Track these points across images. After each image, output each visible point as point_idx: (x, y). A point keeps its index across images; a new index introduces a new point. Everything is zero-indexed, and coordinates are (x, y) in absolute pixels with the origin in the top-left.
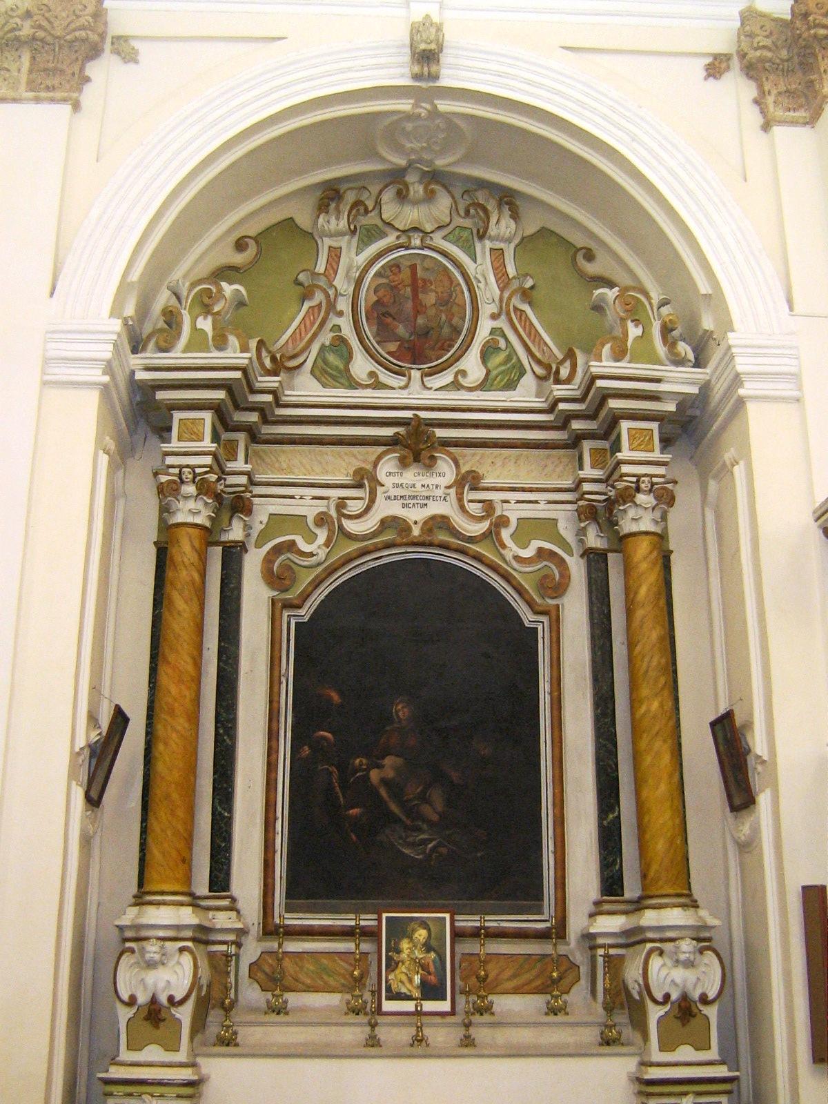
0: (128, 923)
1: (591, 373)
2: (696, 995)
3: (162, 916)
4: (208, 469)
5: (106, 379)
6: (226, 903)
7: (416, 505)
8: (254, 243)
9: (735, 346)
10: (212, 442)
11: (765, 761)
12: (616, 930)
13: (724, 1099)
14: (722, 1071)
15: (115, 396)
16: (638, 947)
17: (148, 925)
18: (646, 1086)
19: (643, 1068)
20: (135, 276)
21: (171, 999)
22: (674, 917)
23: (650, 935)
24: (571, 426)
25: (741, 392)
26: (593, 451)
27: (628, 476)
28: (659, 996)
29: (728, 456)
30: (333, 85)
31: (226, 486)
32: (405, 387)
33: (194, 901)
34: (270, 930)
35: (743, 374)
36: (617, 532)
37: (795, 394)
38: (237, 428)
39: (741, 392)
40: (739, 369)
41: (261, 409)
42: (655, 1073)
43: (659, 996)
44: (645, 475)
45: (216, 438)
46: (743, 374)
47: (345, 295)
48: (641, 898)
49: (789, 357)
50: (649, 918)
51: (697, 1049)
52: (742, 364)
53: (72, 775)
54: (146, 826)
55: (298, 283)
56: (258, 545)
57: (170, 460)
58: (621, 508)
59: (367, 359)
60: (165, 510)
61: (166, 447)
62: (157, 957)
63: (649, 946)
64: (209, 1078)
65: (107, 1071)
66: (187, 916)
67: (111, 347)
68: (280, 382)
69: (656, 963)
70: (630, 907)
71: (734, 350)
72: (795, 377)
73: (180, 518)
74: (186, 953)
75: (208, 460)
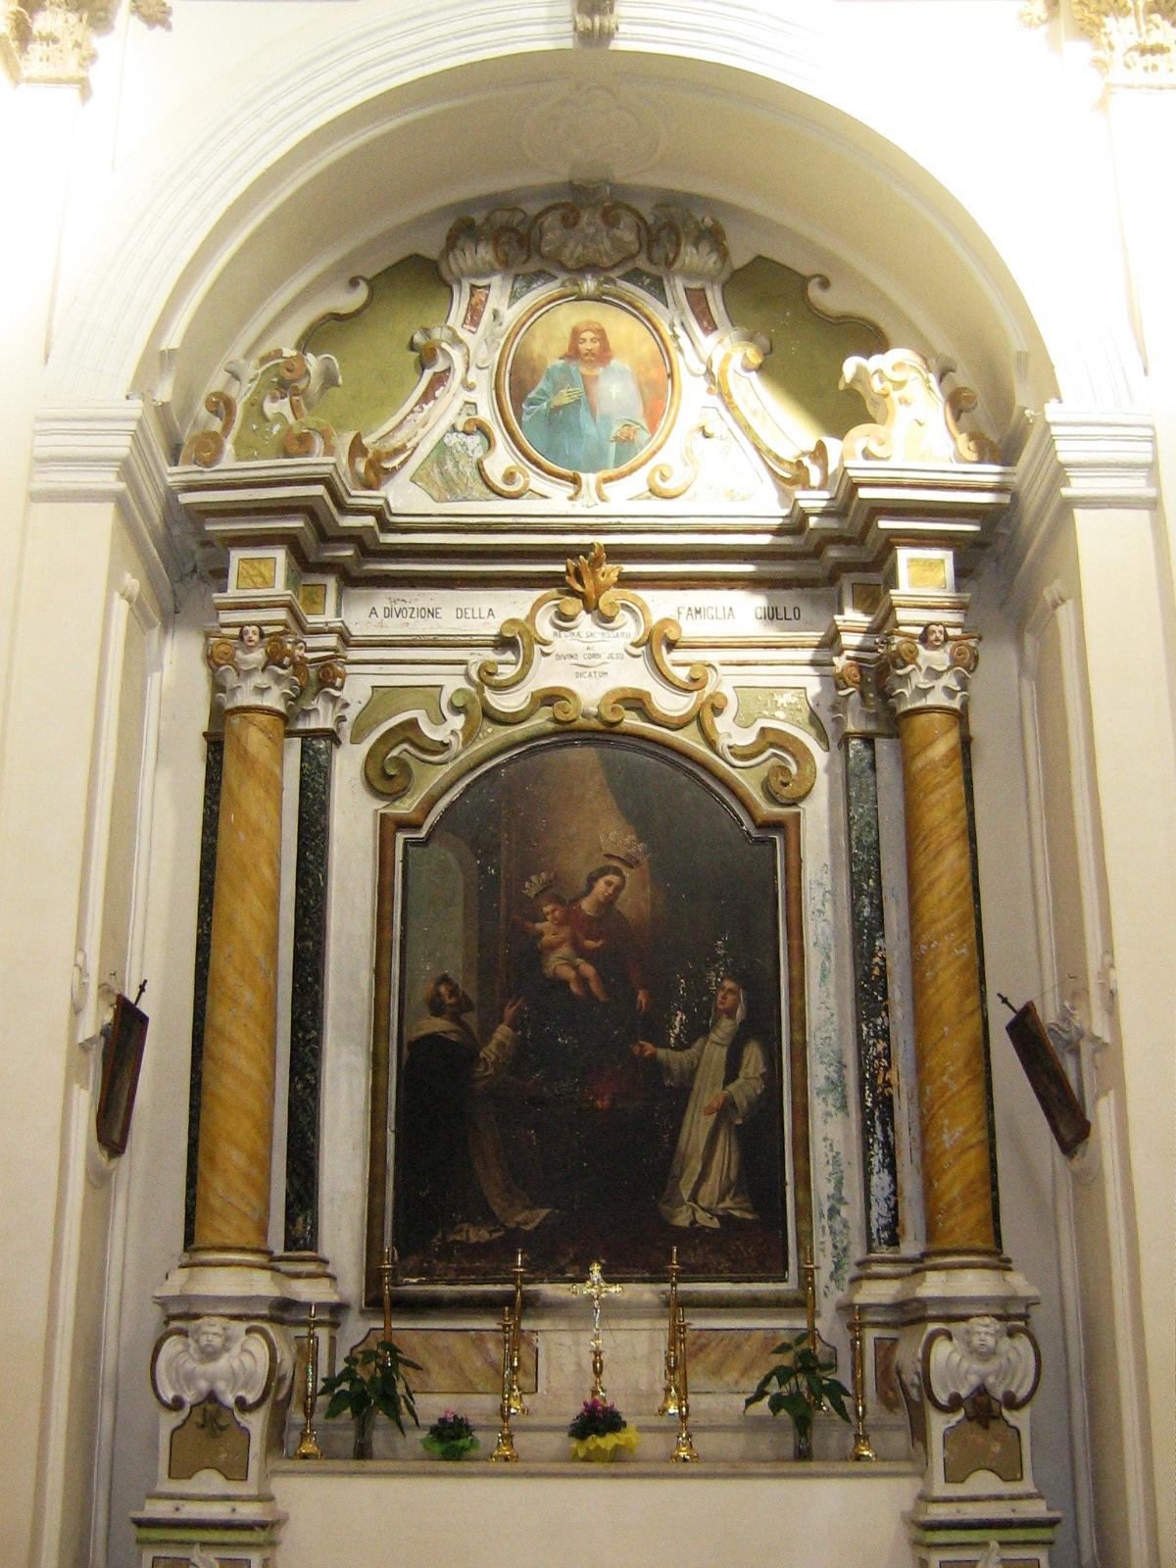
0: (175, 1292)
1: (850, 478)
2: (998, 1393)
3: (223, 1282)
4: (332, 653)
5: (122, 486)
6: (311, 1267)
7: (593, 674)
9: (1055, 424)
10: (287, 589)
11: (1106, 1044)
12: (887, 1300)
13: (1041, 1555)
14: (1037, 1509)
16: (915, 1327)
17: (207, 1297)
18: (924, 1531)
19: (923, 1504)
20: (173, 340)
21: (241, 1402)
22: (974, 1283)
23: (931, 1312)
24: (826, 554)
26: (858, 588)
27: (909, 625)
28: (943, 1398)
29: (1048, 594)
30: (466, 52)
31: (308, 650)
33: (272, 1263)
34: (374, 1303)
36: (893, 710)
37: (1151, 492)
38: (326, 568)
39: (1065, 492)
40: (1062, 457)
41: (353, 537)
42: (940, 1512)
43: (943, 1398)
44: (937, 624)
45: (292, 582)
47: (487, 367)
48: (925, 1255)
49: (1142, 439)
50: (933, 1285)
51: (1005, 1480)
52: (1066, 451)
53: (71, 1076)
55: (412, 347)
56: (356, 739)
57: (226, 617)
58: (899, 672)
59: (544, 478)
60: (218, 686)
61: (218, 597)
62: (217, 1342)
63: (932, 1327)
64: (288, 1519)
65: (143, 1509)
66: (263, 1285)
67: (128, 440)
68: (335, 465)
69: (942, 1350)
70: (908, 1269)
71: (1054, 430)
72: (1151, 469)
73: (245, 698)
74: (258, 1336)
75: (281, 614)
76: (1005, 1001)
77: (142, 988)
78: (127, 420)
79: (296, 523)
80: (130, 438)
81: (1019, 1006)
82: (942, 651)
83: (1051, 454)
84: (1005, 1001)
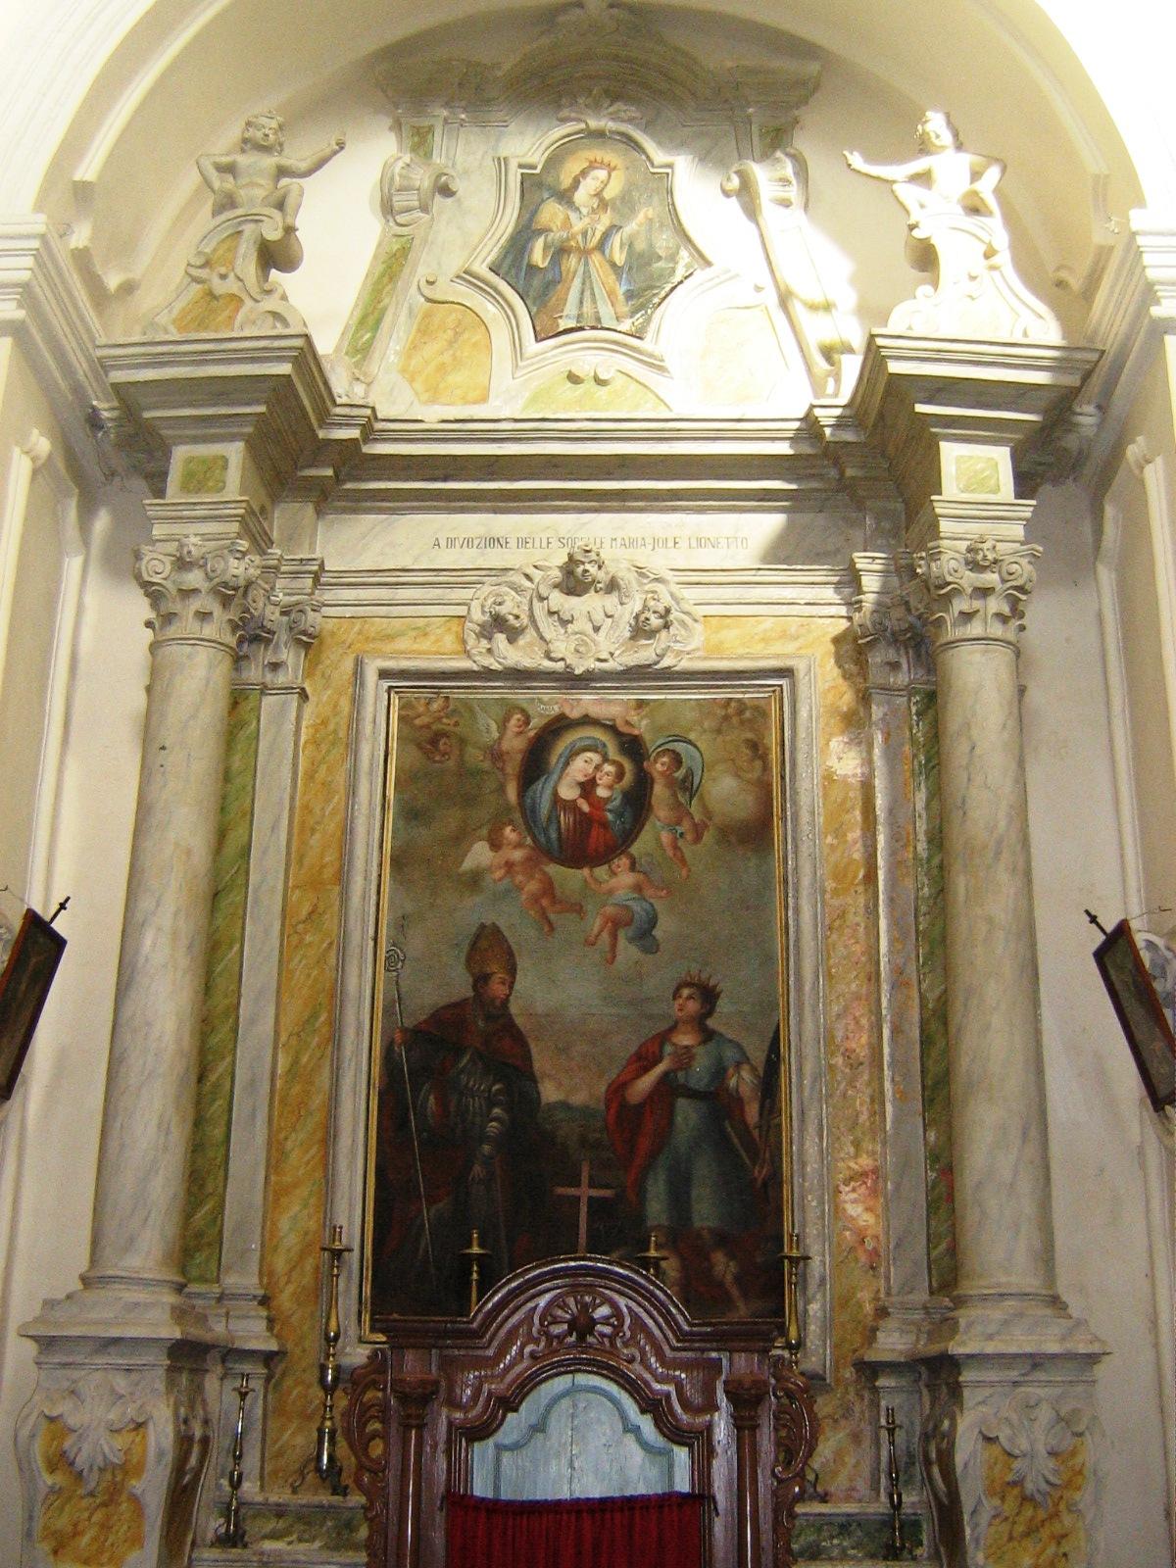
8: (621, 729)
9: (1145, 234)
15: (38, 338)
25: (1156, 311)
32: (813, 406)
35: (1162, 284)
39: (1156, 311)
40: (1151, 274)
46: (1162, 284)
54: (370, 343)
67: (29, 262)
71: (1140, 240)
76: (1093, 919)
77: (62, 906)
78: (28, 237)
79: (490, 1352)
80: (32, 258)
81: (1109, 928)
82: (607, 949)
83: (1138, 271)
84: (1093, 919)
